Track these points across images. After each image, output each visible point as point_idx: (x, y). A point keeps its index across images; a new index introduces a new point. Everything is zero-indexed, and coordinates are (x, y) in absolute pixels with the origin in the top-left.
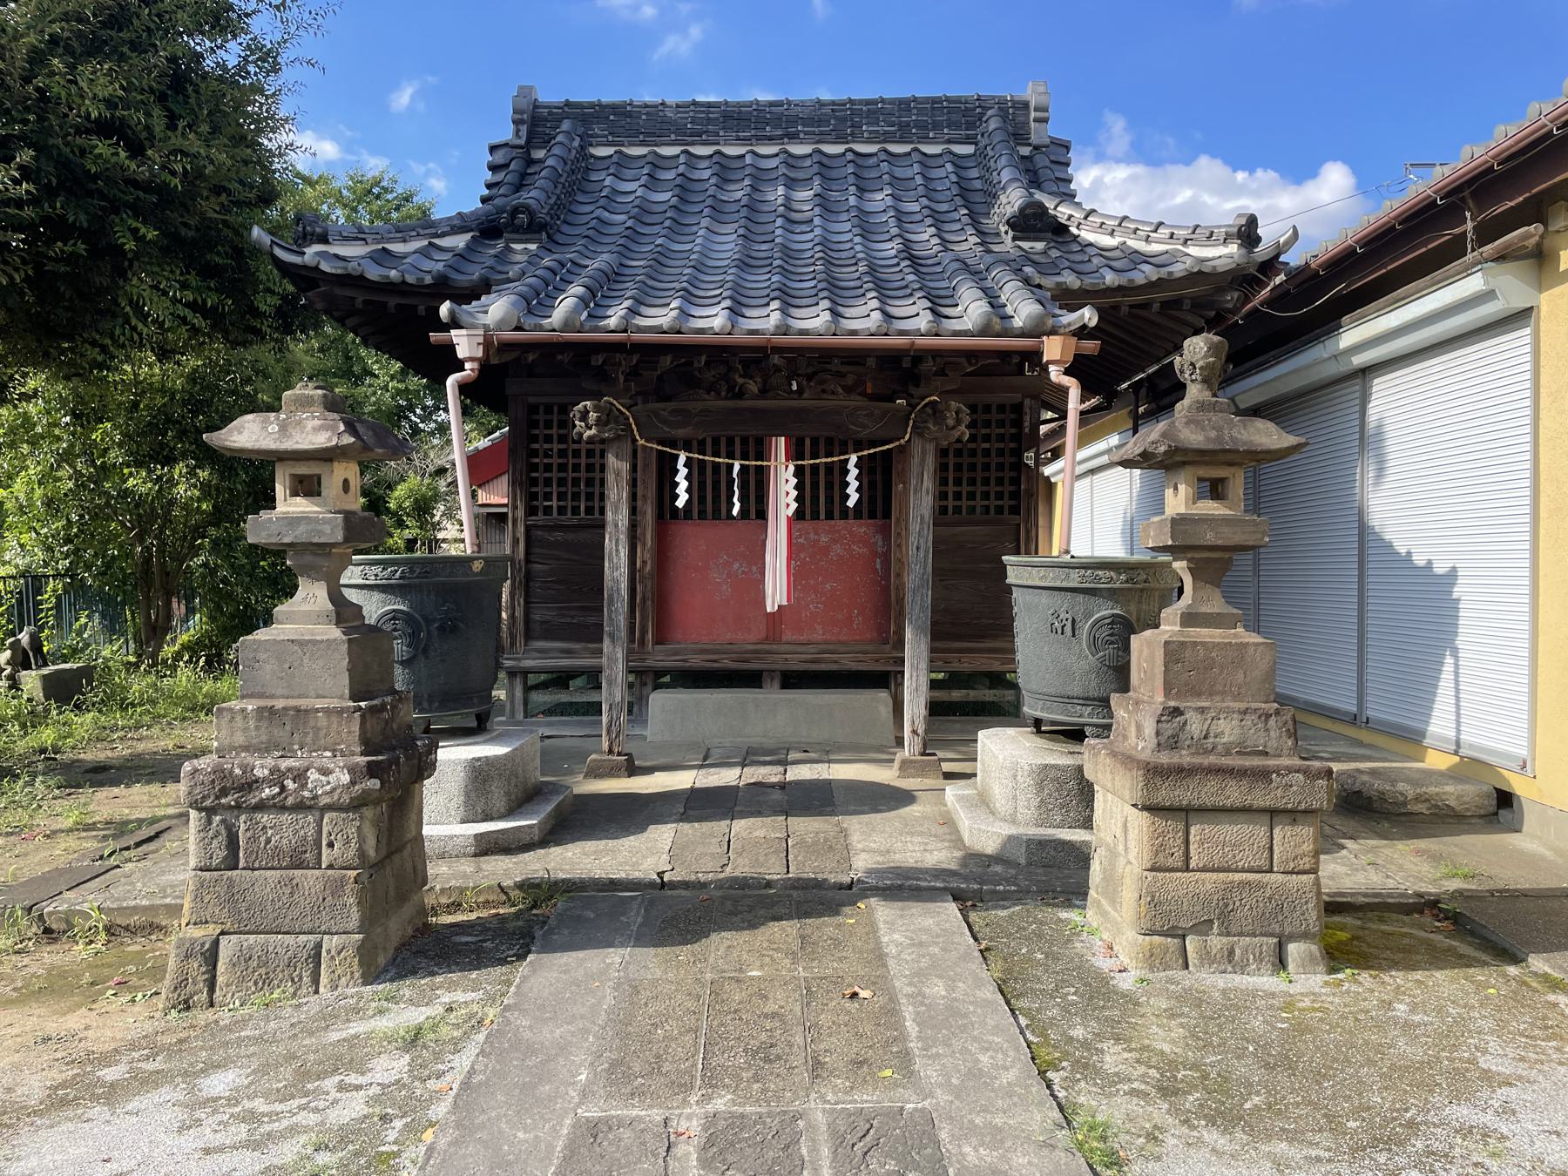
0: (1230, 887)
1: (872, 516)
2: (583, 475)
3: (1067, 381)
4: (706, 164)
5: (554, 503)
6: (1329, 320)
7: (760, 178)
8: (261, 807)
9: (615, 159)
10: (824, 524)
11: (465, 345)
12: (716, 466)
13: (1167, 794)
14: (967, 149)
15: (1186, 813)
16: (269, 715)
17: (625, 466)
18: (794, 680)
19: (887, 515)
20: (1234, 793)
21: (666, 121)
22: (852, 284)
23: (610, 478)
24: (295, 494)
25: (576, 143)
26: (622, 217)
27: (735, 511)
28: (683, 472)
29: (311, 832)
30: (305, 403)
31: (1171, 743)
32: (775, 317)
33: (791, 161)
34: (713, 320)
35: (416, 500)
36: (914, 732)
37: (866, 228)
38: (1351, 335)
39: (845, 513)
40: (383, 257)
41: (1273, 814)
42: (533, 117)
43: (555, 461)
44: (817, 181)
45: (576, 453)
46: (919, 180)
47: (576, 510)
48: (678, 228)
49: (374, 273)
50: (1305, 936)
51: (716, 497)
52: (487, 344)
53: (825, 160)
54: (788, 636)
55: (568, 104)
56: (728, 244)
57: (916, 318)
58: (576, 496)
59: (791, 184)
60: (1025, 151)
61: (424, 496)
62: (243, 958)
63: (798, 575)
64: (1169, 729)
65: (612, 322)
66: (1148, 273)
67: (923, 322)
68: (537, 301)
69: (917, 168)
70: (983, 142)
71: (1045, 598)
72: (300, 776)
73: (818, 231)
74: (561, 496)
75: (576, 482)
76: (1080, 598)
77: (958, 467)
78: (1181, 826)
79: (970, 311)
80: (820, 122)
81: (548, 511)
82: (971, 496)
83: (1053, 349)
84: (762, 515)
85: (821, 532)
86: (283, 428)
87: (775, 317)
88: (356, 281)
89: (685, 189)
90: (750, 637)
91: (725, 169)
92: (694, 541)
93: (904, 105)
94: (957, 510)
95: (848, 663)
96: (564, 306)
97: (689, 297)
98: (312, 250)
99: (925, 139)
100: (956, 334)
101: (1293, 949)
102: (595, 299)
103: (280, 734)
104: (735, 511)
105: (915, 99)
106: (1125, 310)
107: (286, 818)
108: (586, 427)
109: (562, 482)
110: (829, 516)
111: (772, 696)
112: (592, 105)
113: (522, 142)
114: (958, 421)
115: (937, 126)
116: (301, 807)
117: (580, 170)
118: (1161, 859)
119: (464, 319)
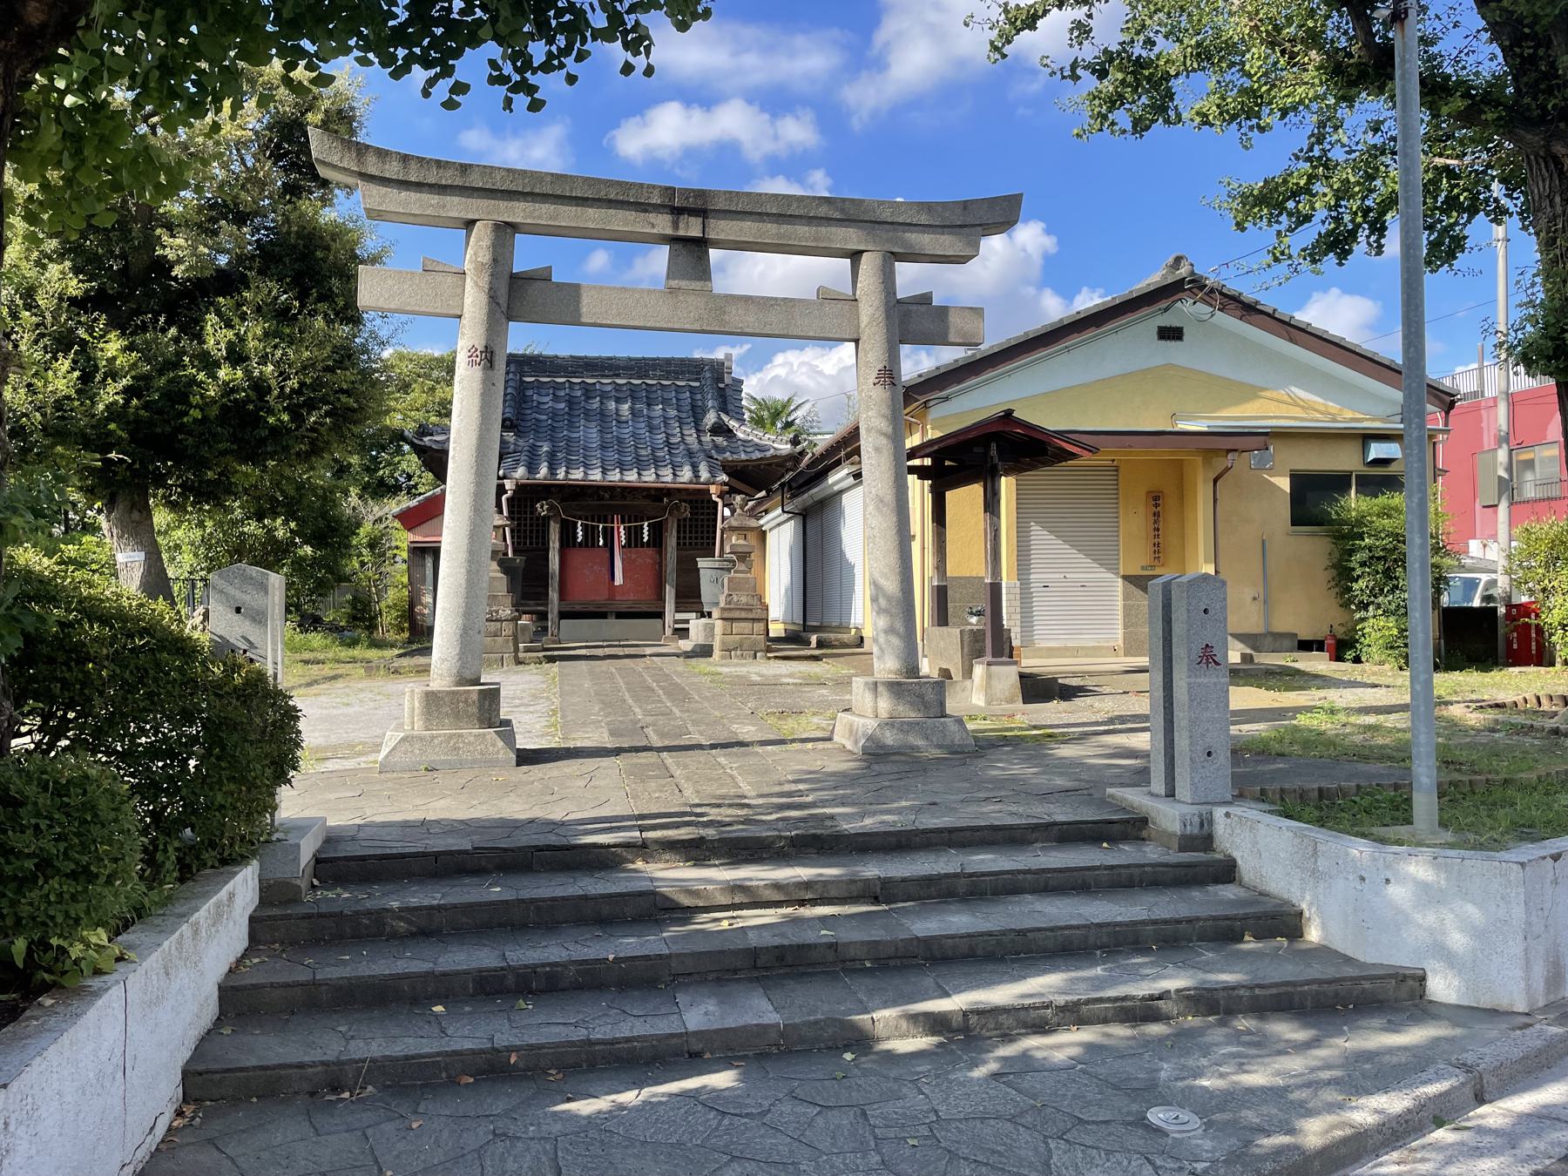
1: (654, 546)
4: (577, 387)
6: (823, 474)
7: (604, 396)
10: (634, 550)
12: (593, 526)
13: (725, 616)
14: (697, 384)
15: (732, 620)
18: (621, 615)
19: (661, 546)
20: (743, 615)
23: (551, 530)
26: (544, 417)
27: (601, 543)
33: (618, 387)
37: (651, 429)
38: (831, 480)
39: (643, 545)
41: (754, 620)
46: (674, 401)
47: (525, 543)
48: (571, 426)
51: (593, 539)
52: (517, 485)
56: (594, 434)
57: (667, 476)
59: (618, 400)
60: (721, 385)
66: (757, 455)
67: (669, 478)
68: (532, 468)
69: (673, 394)
72: (497, 612)
77: (691, 526)
79: (686, 474)
80: (632, 369)
82: (696, 538)
83: (713, 489)
85: (634, 553)
91: (588, 392)
93: (669, 361)
95: (645, 608)
97: (587, 466)
98: (426, 439)
99: (678, 379)
102: (552, 470)
104: (601, 543)
110: (636, 546)
111: (611, 622)
115: (683, 373)
116: (496, 620)
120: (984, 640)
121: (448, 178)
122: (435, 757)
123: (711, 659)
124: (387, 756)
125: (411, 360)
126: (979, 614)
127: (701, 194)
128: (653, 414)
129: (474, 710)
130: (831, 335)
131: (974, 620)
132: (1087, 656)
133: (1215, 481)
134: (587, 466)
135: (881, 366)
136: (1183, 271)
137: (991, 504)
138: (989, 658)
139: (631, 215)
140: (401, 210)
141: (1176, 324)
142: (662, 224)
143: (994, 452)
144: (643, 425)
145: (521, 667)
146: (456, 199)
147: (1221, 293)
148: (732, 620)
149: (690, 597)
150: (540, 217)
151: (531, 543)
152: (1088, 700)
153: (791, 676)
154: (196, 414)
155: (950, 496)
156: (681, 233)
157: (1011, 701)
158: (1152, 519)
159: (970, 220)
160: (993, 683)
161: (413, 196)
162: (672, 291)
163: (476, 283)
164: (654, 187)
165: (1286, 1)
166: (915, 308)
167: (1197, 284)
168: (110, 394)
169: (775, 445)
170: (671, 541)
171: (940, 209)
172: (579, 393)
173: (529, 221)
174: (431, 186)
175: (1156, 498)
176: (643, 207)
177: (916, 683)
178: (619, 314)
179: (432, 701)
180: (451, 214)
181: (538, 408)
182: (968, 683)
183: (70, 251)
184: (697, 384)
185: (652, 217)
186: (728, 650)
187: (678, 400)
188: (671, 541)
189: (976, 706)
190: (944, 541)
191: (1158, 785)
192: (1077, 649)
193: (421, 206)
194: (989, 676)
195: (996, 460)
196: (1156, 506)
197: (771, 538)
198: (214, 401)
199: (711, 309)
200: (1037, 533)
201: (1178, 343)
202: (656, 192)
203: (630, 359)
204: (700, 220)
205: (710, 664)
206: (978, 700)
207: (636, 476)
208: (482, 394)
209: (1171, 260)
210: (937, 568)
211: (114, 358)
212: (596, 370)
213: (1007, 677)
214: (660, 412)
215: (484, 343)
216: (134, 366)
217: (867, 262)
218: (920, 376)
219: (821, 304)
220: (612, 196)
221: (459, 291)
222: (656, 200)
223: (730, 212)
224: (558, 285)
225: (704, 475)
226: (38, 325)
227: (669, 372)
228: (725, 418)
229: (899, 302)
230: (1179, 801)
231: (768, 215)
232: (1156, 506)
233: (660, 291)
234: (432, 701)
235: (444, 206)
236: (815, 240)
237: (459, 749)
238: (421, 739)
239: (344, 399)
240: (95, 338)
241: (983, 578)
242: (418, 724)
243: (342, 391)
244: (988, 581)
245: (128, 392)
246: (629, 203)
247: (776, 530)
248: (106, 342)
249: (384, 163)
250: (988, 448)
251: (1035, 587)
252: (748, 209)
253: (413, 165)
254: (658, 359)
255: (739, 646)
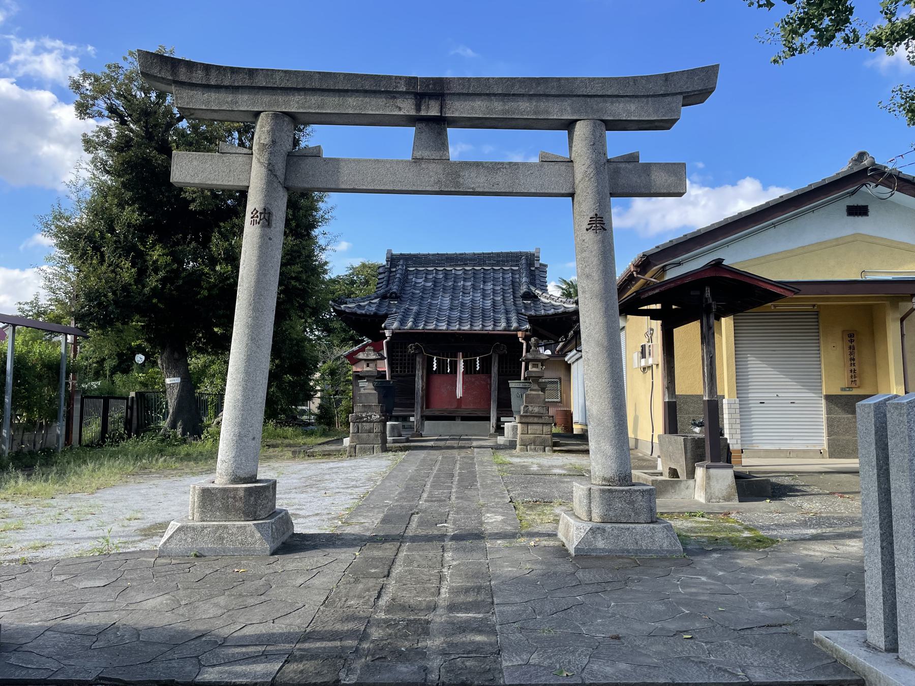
0: (535, 437)
2: (411, 361)
3: (523, 341)
4: (441, 273)
5: (399, 369)
7: (456, 278)
8: (364, 422)
9: (415, 272)
11: (388, 333)
13: (523, 420)
14: (517, 268)
15: (528, 423)
16: (364, 406)
17: (421, 360)
18: (464, 419)
20: (536, 420)
21: (430, 260)
22: (477, 315)
23: (417, 363)
24: (533, 367)
25: (404, 268)
26: (418, 292)
28: (435, 361)
29: (372, 426)
30: (370, 350)
31: (526, 412)
32: (458, 326)
34: (443, 326)
35: (331, 370)
36: (493, 427)
37: (484, 296)
40: (359, 307)
42: (391, 259)
43: (399, 358)
44: (472, 279)
45: (405, 356)
46: (501, 279)
47: (405, 372)
48: (433, 297)
49: (359, 312)
50: (548, 446)
52: (393, 333)
53: (475, 272)
54: (463, 407)
55: (401, 254)
56: (447, 301)
58: (405, 368)
60: (533, 269)
61: (334, 368)
62: (361, 448)
63: (465, 391)
64: (526, 409)
65: (421, 328)
66: (552, 311)
68: (403, 322)
70: (521, 267)
71: (516, 389)
72: (371, 416)
73: (471, 297)
74: (401, 368)
75: (405, 364)
76: (523, 390)
78: (541, 427)
80: (474, 260)
81: (397, 371)
83: (520, 334)
84: (456, 373)
86: (367, 355)
87: (458, 326)
88: (355, 314)
89: (435, 282)
90: (453, 407)
91: (446, 274)
92: (437, 381)
93: (498, 255)
94: (514, 371)
96: (410, 324)
97: (438, 320)
98: (342, 306)
100: (498, 331)
101: (547, 448)
102: (415, 322)
103: (366, 409)
105: (502, 253)
106: (556, 319)
107: (368, 424)
108: (411, 350)
109: (401, 364)
110: (471, 373)
111: (459, 422)
112: (408, 255)
113: (389, 267)
114: (504, 349)
115: (508, 261)
117: (405, 280)
118: (523, 432)
119: (388, 327)
120: (704, 447)
121: (239, 81)
122: (204, 546)
123: (514, 452)
124: (165, 543)
125: (370, 268)
126: (701, 425)
127: (440, 82)
128: (486, 288)
129: (239, 504)
130: (550, 191)
131: (697, 430)
132: (797, 457)
133: (902, 320)
134: (438, 320)
135: (592, 214)
136: (866, 163)
137: (708, 338)
138: (708, 462)
139: (381, 101)
140: (204, 107)
141: (861, 203)
142: (407, 108)
143: (708, 293)
144: (479, 295)
145: (385, 454)
146: (246, 97)
147: (899, 178)
148: (528, 423)
149: (505, 408)
150: (310, 107)
151: (408, 372)
152: (798, 501)
153: (561, 467)
154: (206, 293)
155: (678, 332)
156: (423, 113)
157: (728, 499)
158: (848, 352)
159: (670, 90)
160: (711, 483)
161: (214, 95)
162: (416, 160)
163: (258, 159)
164: (400, 78)
165: (914, 57)
166: (623, 165)
167: (878, 172)
168: (153, 281)
169: (565, 305)
170: (495, 370)
171: (644, 82)
172: (441, 276)
173: (301, 110)
174: (227, 88)
175: (851, 336)
176: (392, 94)
177: (627, 491)
178: (373, 181)
179: (207, 495)
180: (242, 109)
181: (415, 286)
182: (691, 482)
183: (138, 199)
184: (517, 268)
185: (399, 102)
186: (525, 444)
187: (503, 278)
188: (495, 370)
189: (698, 503)
190: (673, 367)
191: (876, 634)
192: (790, 451)
193: (219, 103)
194: (708, 478)
195: (710, 301)
196: (851, 341)
197: (574, 368)
198: (215, 285)
199: (448, 174)
200: (757, 367)
201: (865, 218)
202: (402, 82)
203: (474, 254)
204: (439, 102)
205: (512, 456)
206: (700, 497)
207: (469, 326)
208: (260, 247)
209: (855, 155)
210: (668, 388)
211: (157, 260)
212: (453, 262)
213: (724, 478)
214: (492, 286)
215: (262, 206)
216: (167, 265)
217: (581, 129)
218: (658, 247)
219: (541, 166)
220: (367, 88)
221: (247, 167)
222: (403, 88)
223: (463, 94)
224: (325, 160)
225: (514, 325)
226: (115, 242)
227: (498, 261)
228: (533, 289)
229: (608, 161)
230: (903, 662)
231: (495, 95)
232: (851, 341)
233: (409, 161)
234: (207, 495)
235: (237, 102)
236: (535, 113)
237: (223, 539)
238: (194, 529)
239: (293, 283)
240: (147, 248)
241: (700, 397)
242: (197, 516)
243: (292, 278)
244: (706, 398)
245: (164, 280)
246: (380, 92)
247: (576, 363)
248: (153, 251)
249: (191, 72)
250: (703, 292)
251: (754, 405)
252: (478, 91)
253: (213, 74)
254: (492, 253)
255: (534, 442)
